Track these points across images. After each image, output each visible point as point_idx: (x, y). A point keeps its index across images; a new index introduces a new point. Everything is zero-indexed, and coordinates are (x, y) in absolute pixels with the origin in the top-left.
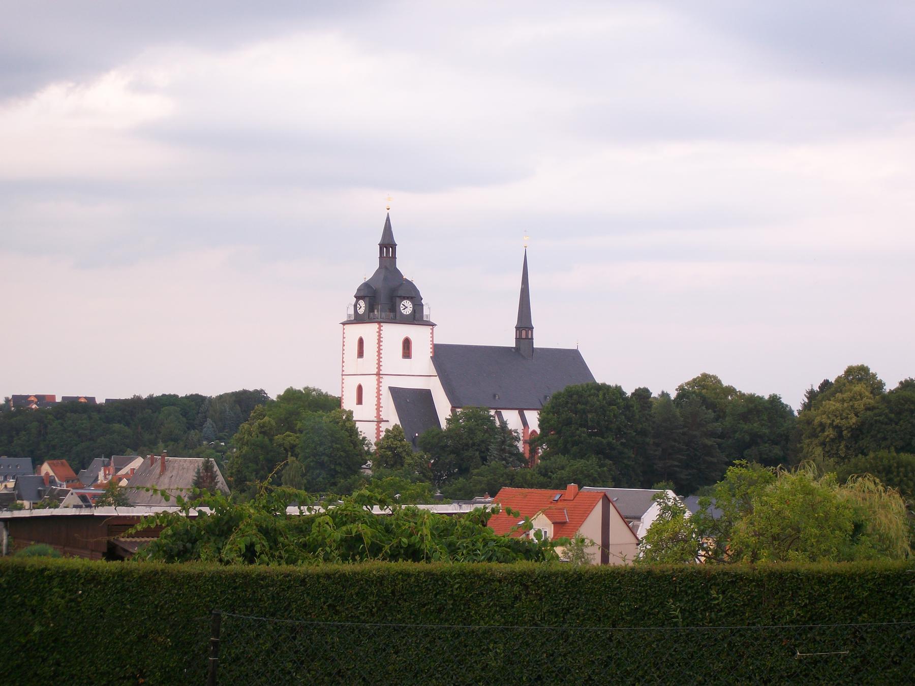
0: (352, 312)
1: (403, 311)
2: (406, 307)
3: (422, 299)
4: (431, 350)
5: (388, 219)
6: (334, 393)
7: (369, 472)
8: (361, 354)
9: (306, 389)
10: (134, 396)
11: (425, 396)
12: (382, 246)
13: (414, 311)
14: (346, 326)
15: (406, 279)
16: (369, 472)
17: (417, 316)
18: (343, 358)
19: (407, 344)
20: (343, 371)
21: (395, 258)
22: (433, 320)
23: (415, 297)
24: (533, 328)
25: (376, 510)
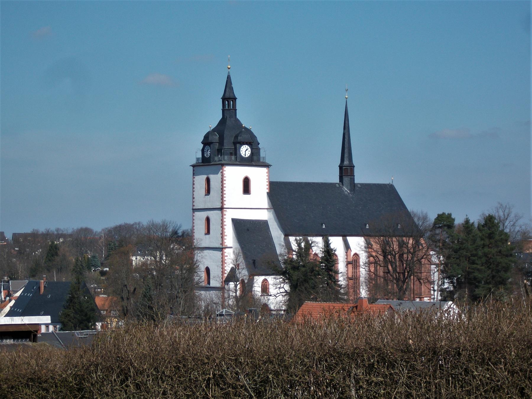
0: (200, 155)
1: (249, 147)
2: (245, 151)
3: (259, 144)
4: (267, 187)
5: (229, 78)
6: (185, 227)
7: (40, 250)
8: (208, 192)
9: (164, 222)
10: (33, 230)
11: (263, 225)
12: (224, 99)
13: (252, 154)
14: (196, 168)
15: (245, 127)
16: (40, 250)
17: (255, 158)
18: (193, 195)
19: (246, 183)
20: (193, 206)
21: (236, 110)
22: (268, 161)
23: (253, 143)
24: (354, 167)
25: (340, 389)
